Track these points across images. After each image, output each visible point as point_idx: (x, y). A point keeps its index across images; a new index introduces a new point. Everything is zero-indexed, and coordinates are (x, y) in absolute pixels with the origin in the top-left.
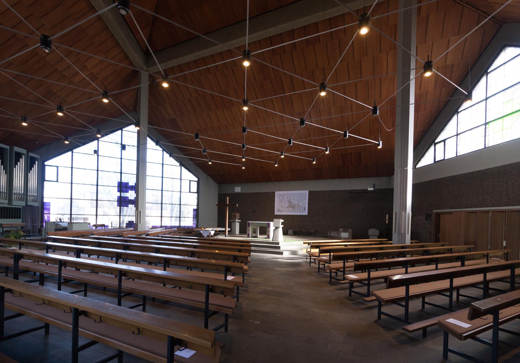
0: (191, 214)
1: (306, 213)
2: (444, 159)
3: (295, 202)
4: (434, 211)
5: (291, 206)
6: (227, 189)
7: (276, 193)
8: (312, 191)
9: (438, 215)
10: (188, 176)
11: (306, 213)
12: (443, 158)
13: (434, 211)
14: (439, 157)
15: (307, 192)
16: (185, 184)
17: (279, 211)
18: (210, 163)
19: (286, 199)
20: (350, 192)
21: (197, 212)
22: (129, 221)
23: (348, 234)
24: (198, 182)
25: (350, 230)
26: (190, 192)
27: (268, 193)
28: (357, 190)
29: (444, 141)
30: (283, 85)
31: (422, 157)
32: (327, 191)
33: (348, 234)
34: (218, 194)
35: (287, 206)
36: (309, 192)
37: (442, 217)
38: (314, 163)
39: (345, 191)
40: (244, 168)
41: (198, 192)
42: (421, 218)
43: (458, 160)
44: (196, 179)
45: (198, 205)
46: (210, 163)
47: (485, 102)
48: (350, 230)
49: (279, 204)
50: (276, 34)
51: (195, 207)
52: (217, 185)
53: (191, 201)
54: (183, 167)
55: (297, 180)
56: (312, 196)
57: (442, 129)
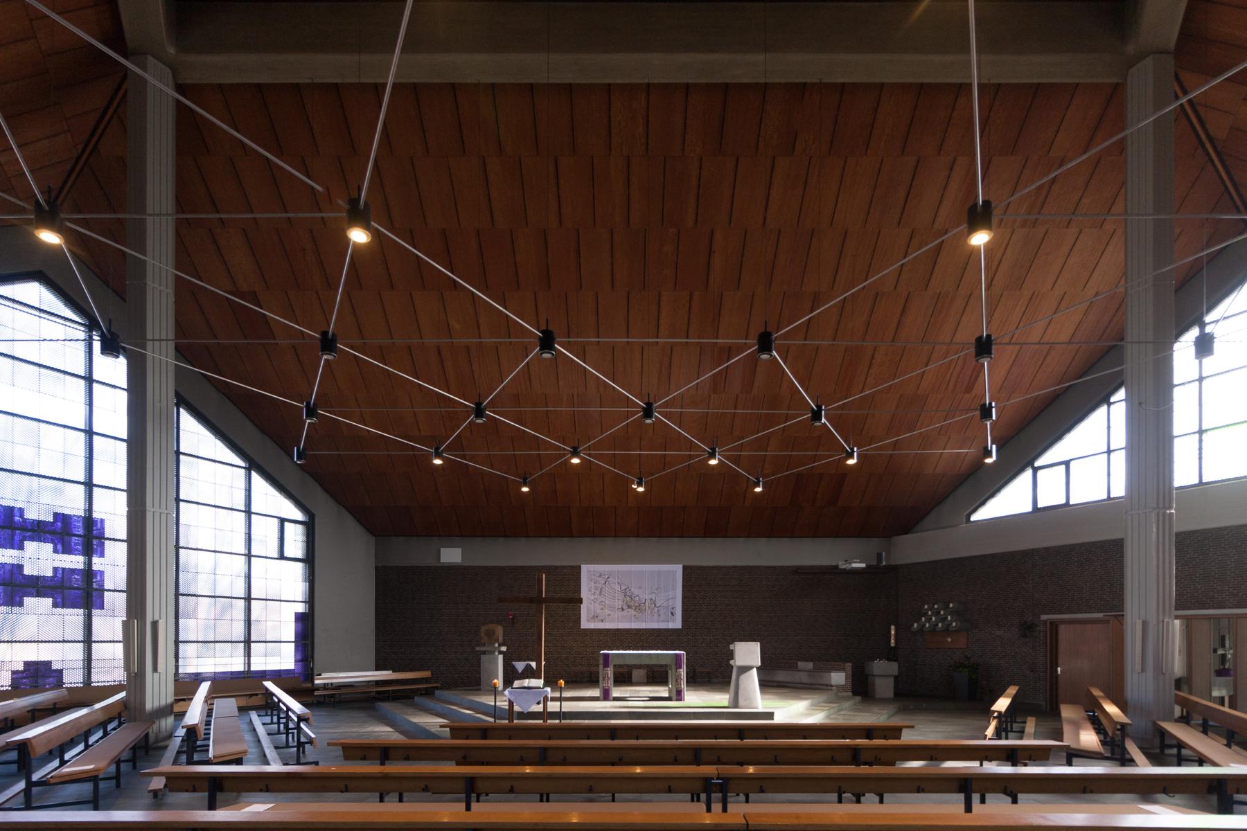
0: (289, 631)
1: (585, 624)
2: (1067, 504)
3: (645, 596)
4: (1044, 617)
5: (632, 604)
6: (412, 553)
7: (585, 569)
8: (691, 567)
9: (1054, 626)
10: (268, 498)
11: (585, 624)
12: (1063, 501)
13: (1044, 617)
14: (1051, 495)
15: (678, 569)
16: (265, 532)
17: (595, 618)
18: (438, 462)
19: (617, 587)
20: (797, 571)
21: (305, 622)
22: (27, 664)
23: (843, 674)
24: (310, 527)
25: (849, 666)
26: (282, 557)
27: (557, 567)
28: (811, 567)
29: (1067, 464)
30: (710, 253)
31: (992, 496)
32: (734, 567)
33: (843, 674)
34: (377, 568)
35: (618, 604)
36: (684, 567)
37: (1062, 628)
38: (758, 490)
39: (782, 568)
40: (525, 489)
41: (309, 560)
42: (998, 633)
43: (1064, 510)
44: (298, 515)
45: (311, 600)
46: (438, 462)
47: (1197, 383)
48: (849, 666)
49: (595, 601)
50: (745, 81)
51: (301, 608)
52: (372, 539)
53: (286, 584)
54: (255, 477)
55: (651, 534)
56: (694, 579)
57: (1059, 438)
